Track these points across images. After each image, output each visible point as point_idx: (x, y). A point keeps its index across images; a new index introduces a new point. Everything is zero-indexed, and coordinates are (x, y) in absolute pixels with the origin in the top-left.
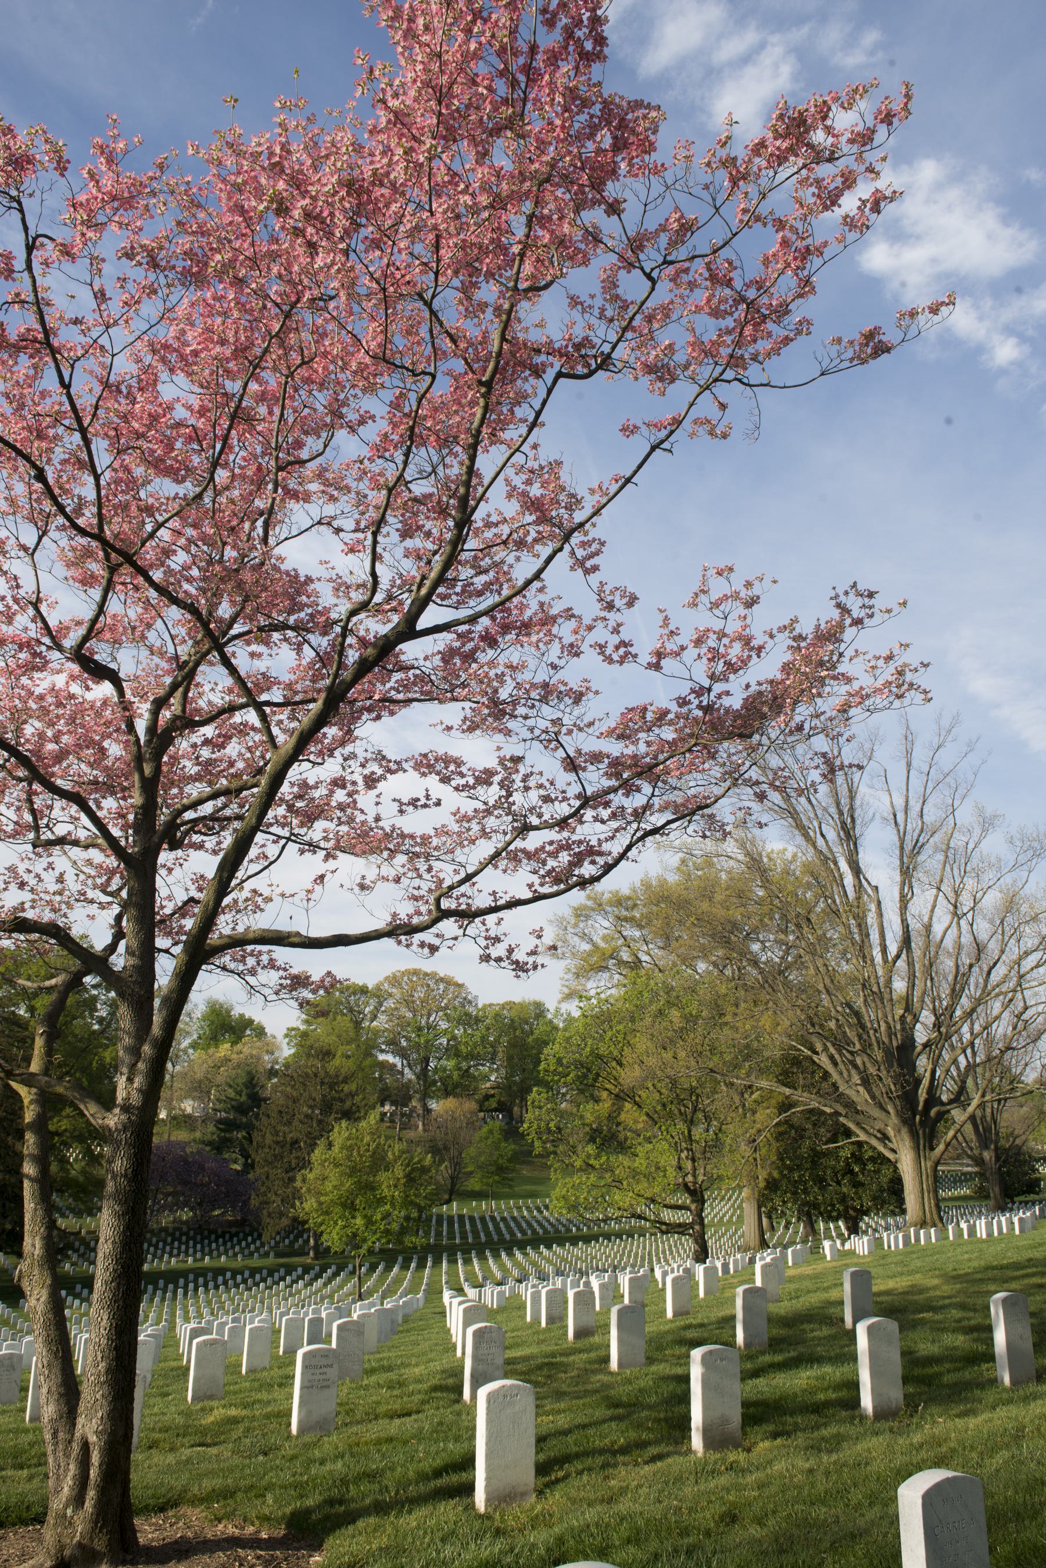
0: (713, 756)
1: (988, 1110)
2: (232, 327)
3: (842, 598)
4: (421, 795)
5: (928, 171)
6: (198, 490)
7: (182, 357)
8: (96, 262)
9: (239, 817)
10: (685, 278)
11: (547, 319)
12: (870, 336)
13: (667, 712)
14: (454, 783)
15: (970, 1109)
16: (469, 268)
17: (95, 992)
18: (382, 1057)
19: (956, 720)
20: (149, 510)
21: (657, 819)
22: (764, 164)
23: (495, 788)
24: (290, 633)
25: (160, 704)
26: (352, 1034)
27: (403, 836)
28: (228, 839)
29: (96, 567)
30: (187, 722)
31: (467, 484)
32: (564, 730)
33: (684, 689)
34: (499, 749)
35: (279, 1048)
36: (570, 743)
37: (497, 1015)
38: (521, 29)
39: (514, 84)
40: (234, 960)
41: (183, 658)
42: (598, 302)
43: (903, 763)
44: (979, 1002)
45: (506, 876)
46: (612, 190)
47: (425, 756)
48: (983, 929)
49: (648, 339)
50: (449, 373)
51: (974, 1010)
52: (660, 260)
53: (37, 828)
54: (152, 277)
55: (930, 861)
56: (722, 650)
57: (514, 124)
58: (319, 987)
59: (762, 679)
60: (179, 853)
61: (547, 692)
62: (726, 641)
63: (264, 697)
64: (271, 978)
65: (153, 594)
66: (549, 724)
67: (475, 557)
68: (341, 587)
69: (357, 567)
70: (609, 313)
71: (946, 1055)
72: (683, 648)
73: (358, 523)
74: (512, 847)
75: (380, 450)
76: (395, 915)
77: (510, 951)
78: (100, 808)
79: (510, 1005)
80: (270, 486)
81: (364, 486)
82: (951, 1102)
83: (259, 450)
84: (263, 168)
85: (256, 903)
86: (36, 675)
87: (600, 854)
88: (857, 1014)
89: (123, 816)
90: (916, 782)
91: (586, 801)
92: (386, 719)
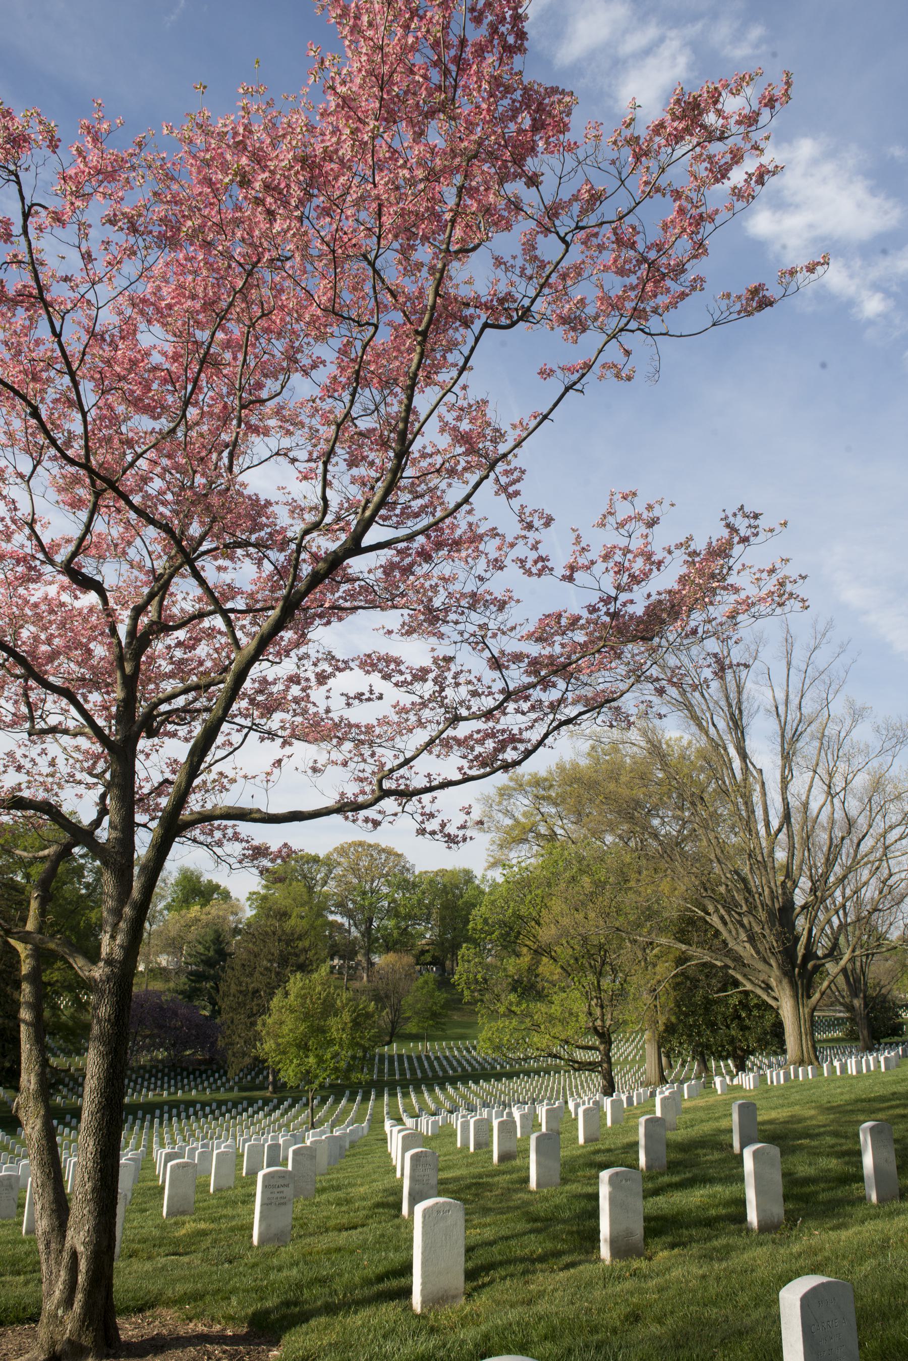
0: (619, 656)
1: (858, 964)
2: (201, 284)
3: (731, 519)
4: (365, 690)
5: (806, 148)
6: (172, 425)
7: (158, 310)
8: (84, 227)
9: (208, 709)
10: (595, 241)
11: (475, 277)
12: (755, 292)
13: (579, 618)
14: (394, 680)
15: (842, 963)
16: (407, 233)
17: (82, 861)
18: (331, 918)
19: (830, 625)
20: (129, 443)
21: (571, 711)
22: (663, 142)
23: (430, 684)
24: (252, 550)
25: (138, 611)
26: (305, 898)
27: (350, 725)
28: (198, 728)
29: (83, 493)
30: (162, 627)
31: (406, 420)
32: (490, 634)
33: (594, 598)
34: (433, 650)
35: (242, 910)
36: (495, 645)
37: (431, 881)
38: (452, 25)
39: (446, 73)
40: (203, 833)
41: (159, 571)
42: (519, 262)
43: (784, 662)
44: (850, 869)
45: (439, 761)
46: (531, 165)
47: (369, 656)
48: (853, 806)
49: (563, 294)
51: (845, 877)
52: (573, 225)
53: (32, 719)
54: (132, 240)
55: (807, 747)
56: (627, 564)
57: (446, 108)
58: (277, 857)
59: (661, 589)
60: (156, 740)
61: (475, 601)
62: (630, 556)
63: (229, 605)
64: (236, 849)
65: (132, 515)
66: (476, 629)
67: (413, 484)
68: (296, 509)
69: (310, 492)
70: (529, 272)
71: (821, 916)
72: (593, 563)
73: (311, 454)
74: (444, 735)
75: (330, 391)
76: (342, 794)
77: (443, 825)
78: (86, 701)
79: (443, 872)
81: (316, 422)
82: (825, 956)
83: (225, 390)
84: (228, 146)
85: (222, 783)
86: (32, 586)
87: (521, 741)
88: (744, 880)
89: (107, 708)
90: (796, 679)
91: (509, 695)
92: (335, 624)
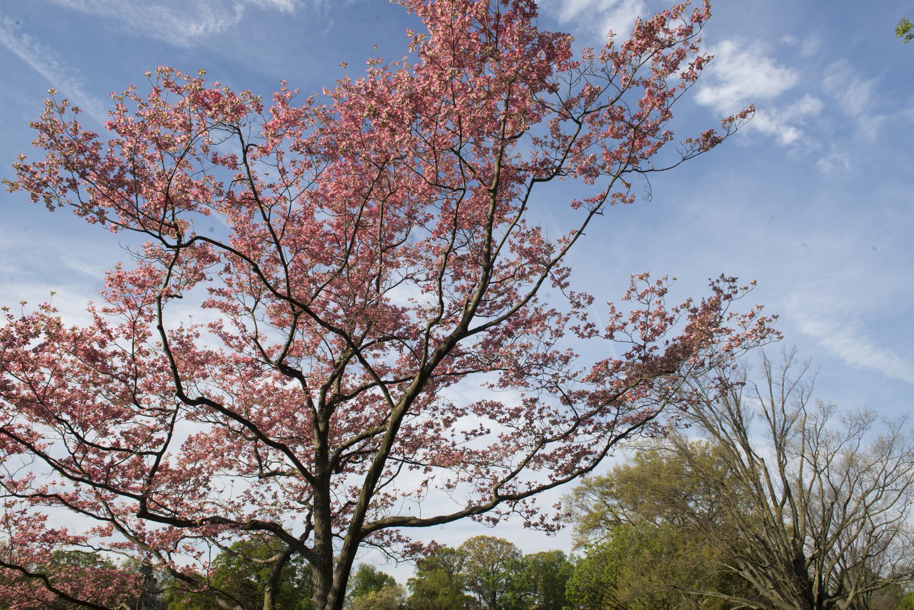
0: (651, 387)
1: (861, 599)
2: (351, 179)
3: (716, 284)
4: (478, 428)
5: (727, 47)
6: (339, 268)
7: (326, 199)
8: (280, 154)
9: (375, 451)
10: (597, 120)
11: (522, 153)
12: (708, 135)
13: (621, 363)
14: (498, 418)
15: (849, 599)
16: (478, 132)
17: (294, 564)
18: (467, 594)
19: (794, 350)
20: (314, 281)
21: (622, 429)
22: (633, 53)
23: (522, 419)
24: (395, 341)
25: (326, 388)
26: (447, 580)
27: (471, 453)
28: (369, 465)
29: (285, 316)
30: (342, 397)
31: (489, 247)
32: (560, 380)
33: (629, 348)
34: (523, 395)
35: (404, 592)
36: (566, 387)
37: (535, 562)
38: (490, 7)
39: (490, 35)
40: (376, 538)
41: (337, 361)
42: (550, 139)
43: (766, 380)
44: (842, 527)
45: (535, 472)
46: (549, 80)
47: (480, 403)
48: (836, 479)
49: (579, 156)
50: (471, 188)
51: (839, 533)
52: (582, 112)
53: (261, 467)
54: (309, 158)
55: (794, 439)
56: (649, 323)
57: (495, 54)
58: (428, 551)
59: (675, 337)
60: (341, 475)
61: (548, 360)
62: (650, 317)
63: (383, 379)
64: (399, 547)
65: (319, 327)
66: (550, 377)
67: (495, 287)
68: (421, 312)
69: (432, 299)
70: (556, 144)
71: (826, 565)
72: (625, 324)
73: (427, 275)
74: (537, 454)
75: (438, 233)
76: (470, 502)
77: (542, 518)
78: (295, 452)
79: (542, 554)
80: (378, 261)
81: (430, 255)
82: (835, 595)
83: (370, 242)
84: (363, 96)
85: (388, 501)
86: (257, 379)
87: (591, 453)
88: (763, 542)
89: (308, 456)
90: (777, 391)
91: (579, 421)
92: (453, 385)
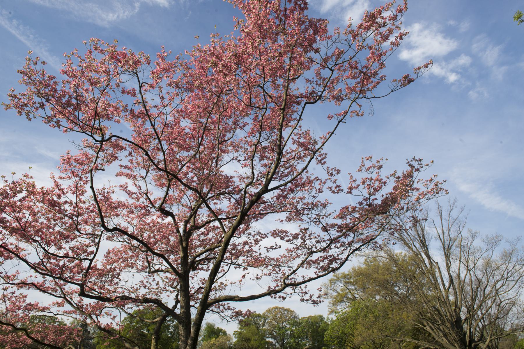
0: (373, 221)
1: (494, 343)
2: (201, 103)
3: (411, 163)
4: (274, 245)
5: (417, 27)
6: (194, 153)
7: (187, 114)
8: (160, 88)
9: (215, 258)
10: (342, 69)
11: (299, 87)
12: (406, 77)
13: (356, 207)
14: (285, 239)
15: (487, 343)
16: (274, 75)
17: (169, 323)
18: (267, 340)
19: (455, 200)
20: (180, 161)
21: (357, 246)
22: (363, 30)
23: (300, 240)
24: (227, 195)
25: (187, 222)
26: (256, 332)
27: (270, 259)
28: (211, 266)
29: (164, 181)
30: (196, 227)
31: (280, 141)
32: (321, 218)
33: (361, 199)
34: (300, 226)
35: (232, 339)
36: (324, 221)
37: (307, 321)
38: (281, 4)
39: (281, 20)
40: (216, 308)
41: (193, 207)
42: (315, 79)
43: (439, 217)
44: (482, 301)
45: (307, 270)
46: (315, 46)
47: (275, 231)
48: (479, 274)
49: (332, 89)
50: (270, 108)
51: (481, 305)
52: (334, 64)
53: (150, 267)
54: (177, 90)
55: (455, 251)
56: (372, 185)
57: (284, 31)
58: (245, 315)
59: (387, 193)
60: (195, 272)
61: (314, 206)
62: (373, 181)
63: (219, 217)
64: (229, 313)
65: (183, 187)
66: (315, 216)
67: (284, 164)
68: (241, 178)
69: (248, 171)
70: (319, 83)
71: (474, 323)
72: (358, 185)
73: (245, 157)
74: (308, 260)
75: (251, 134)
76: (270, 287)
77: (311, 297)
78: (169, 259)
79: (311, 317)
81: (246, 146)
82: (479, 341)
83: (212, 139)
84: (208, 55)
85: (222, 287)
86: (147, 217)
87: (339, 259)
88: (438, 310)
89: (176, 261)
90: (445, 224)
91: (332, 241)
92: (260, 220)
